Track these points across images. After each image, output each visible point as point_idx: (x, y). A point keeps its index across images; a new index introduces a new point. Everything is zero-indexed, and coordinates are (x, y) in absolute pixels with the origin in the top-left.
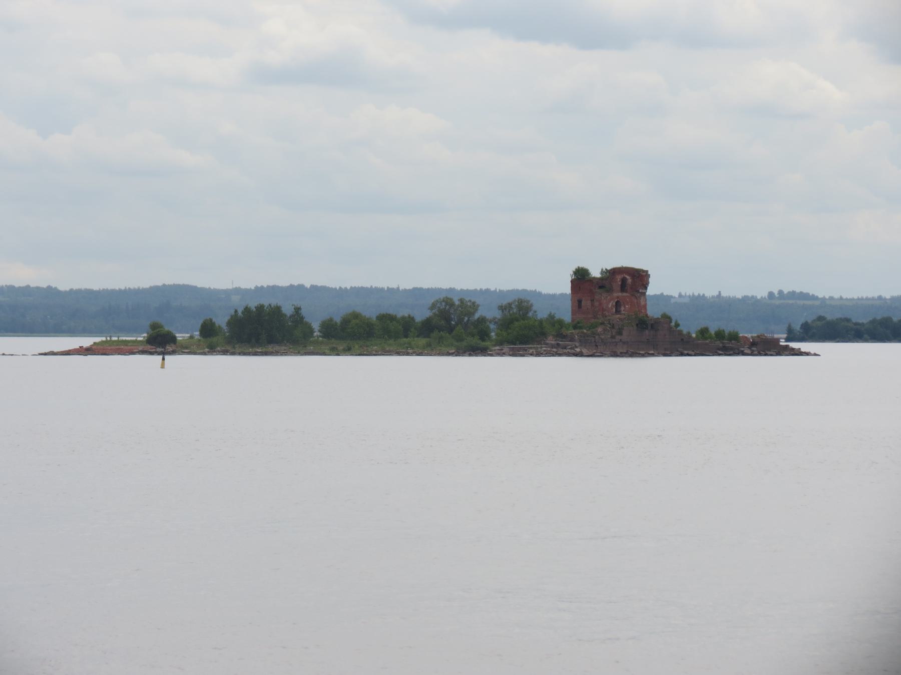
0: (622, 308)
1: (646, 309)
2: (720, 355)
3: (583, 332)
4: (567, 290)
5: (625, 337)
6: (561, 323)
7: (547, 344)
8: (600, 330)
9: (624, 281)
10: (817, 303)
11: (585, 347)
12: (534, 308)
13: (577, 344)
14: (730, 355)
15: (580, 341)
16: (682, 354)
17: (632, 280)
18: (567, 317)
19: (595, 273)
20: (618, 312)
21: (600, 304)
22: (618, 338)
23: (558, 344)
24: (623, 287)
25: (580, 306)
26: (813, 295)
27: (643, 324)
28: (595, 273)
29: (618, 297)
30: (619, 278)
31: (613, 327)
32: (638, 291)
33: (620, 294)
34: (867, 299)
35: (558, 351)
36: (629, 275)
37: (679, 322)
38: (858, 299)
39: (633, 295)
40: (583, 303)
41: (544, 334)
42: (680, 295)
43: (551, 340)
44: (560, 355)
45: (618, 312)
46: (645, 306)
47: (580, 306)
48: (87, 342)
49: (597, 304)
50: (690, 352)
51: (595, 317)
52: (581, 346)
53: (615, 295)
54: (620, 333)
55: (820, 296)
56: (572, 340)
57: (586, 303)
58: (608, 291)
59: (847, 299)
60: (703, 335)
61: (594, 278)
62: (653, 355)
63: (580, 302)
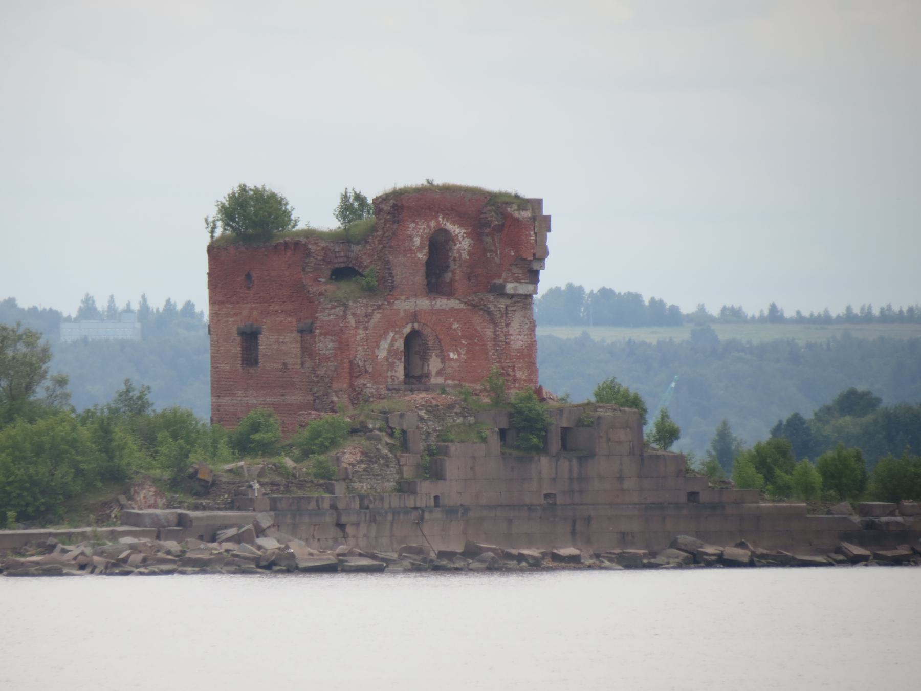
0: (434, 364)
1: (531, 366)
2: (854, 561)
3: (278, 469)
4: (187, 284)
5: (452, 488)
6: (177, 425)
7: (135, 520)
8: (350, 455)
9: (439, 245)
10: (681, 335)
11: (294, 530)
12: (54, 368)
13: (265, 520)
14: (897, 562)
15: (274, 506)
16: (695, 560)
17: (476, 243)
18: (196, 400)
19: (315, 212)
20: (415, 379)
21: (343, 346)
22: (427, 488)
23: (182, 521)
24: (436, 271)
25: (250, 356)
26: (657, 305)
27: (527, 429)
28: (315, 212)
29: (414, 316)
30: (418, 233)
31: (404, 443)
32: (499, 291)
33: (424, 303)
34: (887, 317)
35: (184, 549)
36: (461, 217)
37: (676, 420)
38: (849, 318)
39: (475, 307)
40: (265, 344)
41: (117, 478)
42: (88, 310)
43: (149, 504)
44: (203, 567)
45: (415, 379)
46: (528, 355)
47: (250, 356)
48: (705, 557)
49: (326, 345)
50: (731, 551)
51: (320, 403)
52: (277, 525)
53: (404, 305)
54: (433, 470)
55: (687, 308)
56: (239, 500)
57: (278, 343)
58: (370, 291)
59: (800, 320)
60: (769, 477)
61: (310, 234)
62: (574, 563)
63: (250, 337)
